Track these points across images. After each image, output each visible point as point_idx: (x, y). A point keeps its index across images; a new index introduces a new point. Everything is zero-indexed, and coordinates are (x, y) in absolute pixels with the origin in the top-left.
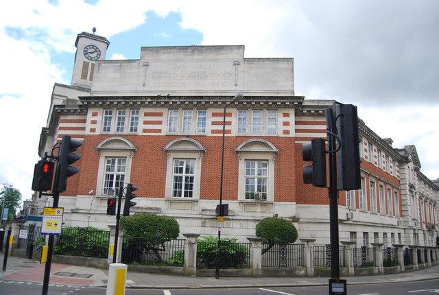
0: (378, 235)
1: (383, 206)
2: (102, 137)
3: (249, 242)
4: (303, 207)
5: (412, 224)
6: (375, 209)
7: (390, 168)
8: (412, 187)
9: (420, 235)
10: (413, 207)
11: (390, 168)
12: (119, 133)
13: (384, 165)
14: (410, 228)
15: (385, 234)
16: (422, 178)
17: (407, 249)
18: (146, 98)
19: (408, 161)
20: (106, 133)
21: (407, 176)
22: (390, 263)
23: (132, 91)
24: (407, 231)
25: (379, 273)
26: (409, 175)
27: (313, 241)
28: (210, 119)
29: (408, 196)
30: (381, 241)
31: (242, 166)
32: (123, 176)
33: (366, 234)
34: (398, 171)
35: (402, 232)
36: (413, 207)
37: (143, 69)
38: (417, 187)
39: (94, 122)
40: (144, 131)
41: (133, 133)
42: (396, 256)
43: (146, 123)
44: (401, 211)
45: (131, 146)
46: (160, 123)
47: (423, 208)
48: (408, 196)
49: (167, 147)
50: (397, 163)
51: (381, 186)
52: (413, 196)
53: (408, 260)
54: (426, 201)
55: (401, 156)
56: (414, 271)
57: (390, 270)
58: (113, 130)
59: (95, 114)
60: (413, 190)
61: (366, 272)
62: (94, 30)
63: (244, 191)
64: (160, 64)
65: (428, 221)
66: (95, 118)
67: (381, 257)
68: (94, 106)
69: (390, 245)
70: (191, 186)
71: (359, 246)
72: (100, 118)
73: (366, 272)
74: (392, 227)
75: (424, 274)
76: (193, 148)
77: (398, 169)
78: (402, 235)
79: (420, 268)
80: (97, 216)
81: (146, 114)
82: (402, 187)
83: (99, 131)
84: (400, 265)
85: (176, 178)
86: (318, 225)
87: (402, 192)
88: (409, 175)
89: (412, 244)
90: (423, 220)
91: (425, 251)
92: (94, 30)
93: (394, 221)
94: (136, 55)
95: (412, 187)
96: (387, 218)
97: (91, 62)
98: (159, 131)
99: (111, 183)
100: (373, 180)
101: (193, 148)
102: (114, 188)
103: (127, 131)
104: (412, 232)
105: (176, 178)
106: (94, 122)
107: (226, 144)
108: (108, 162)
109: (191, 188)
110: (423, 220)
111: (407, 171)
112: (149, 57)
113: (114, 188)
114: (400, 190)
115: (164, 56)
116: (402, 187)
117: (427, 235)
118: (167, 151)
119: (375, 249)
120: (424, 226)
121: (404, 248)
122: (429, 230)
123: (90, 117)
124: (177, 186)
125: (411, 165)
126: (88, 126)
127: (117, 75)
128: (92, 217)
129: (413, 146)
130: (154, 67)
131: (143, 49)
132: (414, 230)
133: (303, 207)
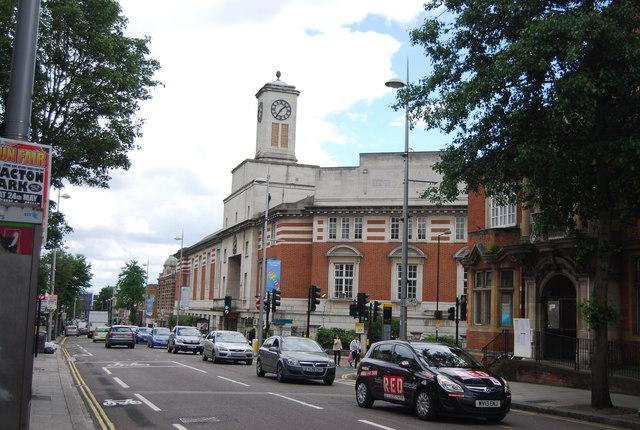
2: (329, 245)
12: (345, 240)
15: (214, 316)
18: (369, 207)
20: (332, 240)
23: (354, 200)
28: (429, 227)
31: (332, 270)
32: (351, 280)
37: (362, 177)
39: (320, 230)
40: (369, 238)
41: (358, 240)
43: (369, 230)
45: (358, 254)
46: (383, 230)
49: (456, 255)
58: (339, 238)
59: (320, 222)
62: (278, 75)
63: (417, 287)
64: (378, 170)
66: (321, 226)
68: (321, 214)
70: (415, 289)
72: (326, 226)
76: (348, 253)
80: (331, 318)
81: (433, 222)
83: (326, 239)
85: (337, 280)
92: (278, 75)
94: (356, 163)
97: (281, 122)
98: (383, 238)
99: (341, 287)
101: (348, 253)
102: (344, 291)
103: (352, 239)
105: (337, 280)
106: (320, 230)
107: (441, 249)
108: (337, 268)
109: (351, 290)
112: (368, 164)
113: (344, 291)
115: (383, 163)
118: (328, 257)
123: (316, 226)
124: (339, 288)
126: (316, 234)
127: (338, 183)
128: (327, 319)
130: (373, 174)
131: (362, 155)
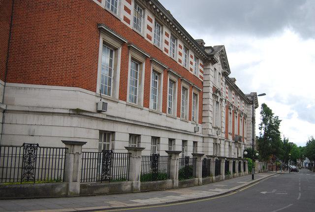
0: (197, 144)
1: (186, 112)
3: (64, 146)
4: (20, 88)
5: (213, 132)
6: (159, 108)
7: (193, 66)
8: (216, 91)
9: (222, 146)
10: (216, 115)
11: (193, 66)
13: (239, 105)
14: (210, 136)
16: (231, 84)
17: (205, 159)
19: (214, 62)
21: (212, 79)
22: (187, 173)
24: (206, 140)
25: (132, 191)
26: (213, 77)
27: (81, 144)
29: (210, 101)
30: (178, 147)
33: (184, 142)
34: (201, 71)
35: (199, 140)
36: (216, 115)
38: (224, 95)
42: (129, 168)
44: (201, 117)
47: (230, 118)
48: (210, 101)
50: (200, 62)
51: (195, 95)
52: (217, 103)
53: (206, 173)
54: (235, 112)
55: (208, 55)
56: (195, 185)
57: (154, 185)
60: (218, 95)
61: (106, 190)
65: (236, 132)
67: (177, 166)
69: (189, 154)
71: (147, 152)
73: (106, 190)
74: (185, 133)
75: (159, 197)
77: (202, 69)
78: (199, 144)
79: (204, 183)
82: (205, 90)
84: (173, 179)
86: (42, 117)
87: (205, 96)
88: (213, 77)
89: (211, 154)
90: (230, 131)
91: (234, 163)
93: (190, 127)
95: (216, 91)
96: (178, 120)
100: (175, 79)
104: (212, 141)
110: (230, 131)
111: (212, 73)
114: (202, 93)
116: (205, 90)
117: (233, 147)
119: (170, 157)
120: (230, 138)
121: (202, 159)
122: (236, 142)
125: (218, 67)
129: (222, 46)
132: (215, 139)
133: (20, 88)
